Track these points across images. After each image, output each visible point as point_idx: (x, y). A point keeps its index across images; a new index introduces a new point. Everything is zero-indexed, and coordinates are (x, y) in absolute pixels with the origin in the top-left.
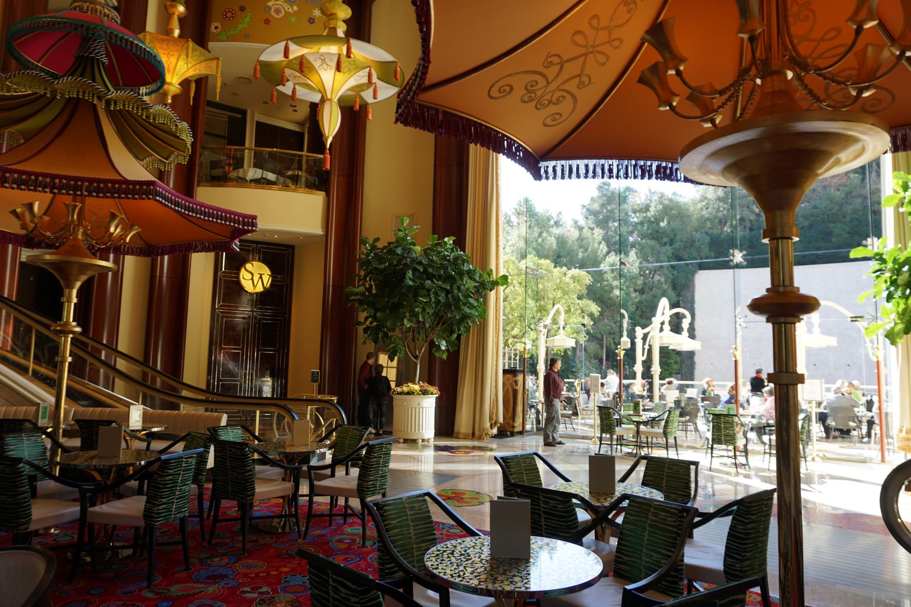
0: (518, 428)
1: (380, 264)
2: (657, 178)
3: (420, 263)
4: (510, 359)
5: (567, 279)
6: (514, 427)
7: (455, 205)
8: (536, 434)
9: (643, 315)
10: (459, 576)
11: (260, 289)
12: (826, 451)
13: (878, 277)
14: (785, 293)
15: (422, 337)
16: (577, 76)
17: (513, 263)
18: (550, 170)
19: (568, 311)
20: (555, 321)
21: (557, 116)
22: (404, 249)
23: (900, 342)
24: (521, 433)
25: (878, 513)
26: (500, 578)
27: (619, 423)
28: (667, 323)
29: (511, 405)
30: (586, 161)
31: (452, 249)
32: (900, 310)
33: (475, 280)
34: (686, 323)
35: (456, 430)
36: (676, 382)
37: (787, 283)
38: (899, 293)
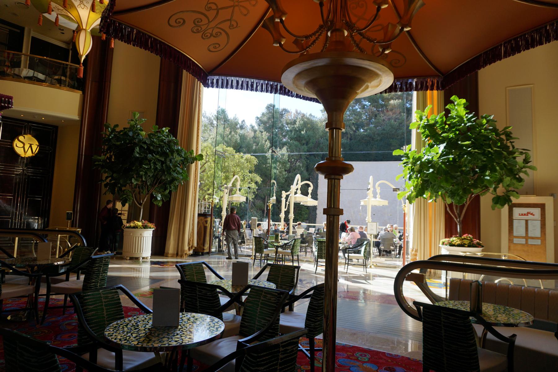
0: (207, 250)
1: (117, 142)
2: (280, 94)
3: (145, 143)
4: (205, 208)
5: (243, 160)
6: (204, 249)
7: (173, 109)
8: (218, 254)
9: (286, 185)
10: (125, 340)
11: (29, 154)
12: (379, 263)
13: (405, 166)
14: (335, 161)
15: (145, 191)
16: (228, 20)
17: (210, 148)
18: (215, 81)
19: (243, 180)
20: (234, 185)
21: (217, 46)
22: (134, 133)
23: (414, 202)
24: (209, 253)
25: (392, 293)
26: (153, 339)
27: (266, 247)
28: (299, 189)
29: (203, 236)
30: (237, 79)
31: (168, 136)
32: (415, 185)
33: (181, 156)
34: (310, 190)
35: (166, 251)
36: (304, 224)
37: (337, 155)
38: (414, 176)
